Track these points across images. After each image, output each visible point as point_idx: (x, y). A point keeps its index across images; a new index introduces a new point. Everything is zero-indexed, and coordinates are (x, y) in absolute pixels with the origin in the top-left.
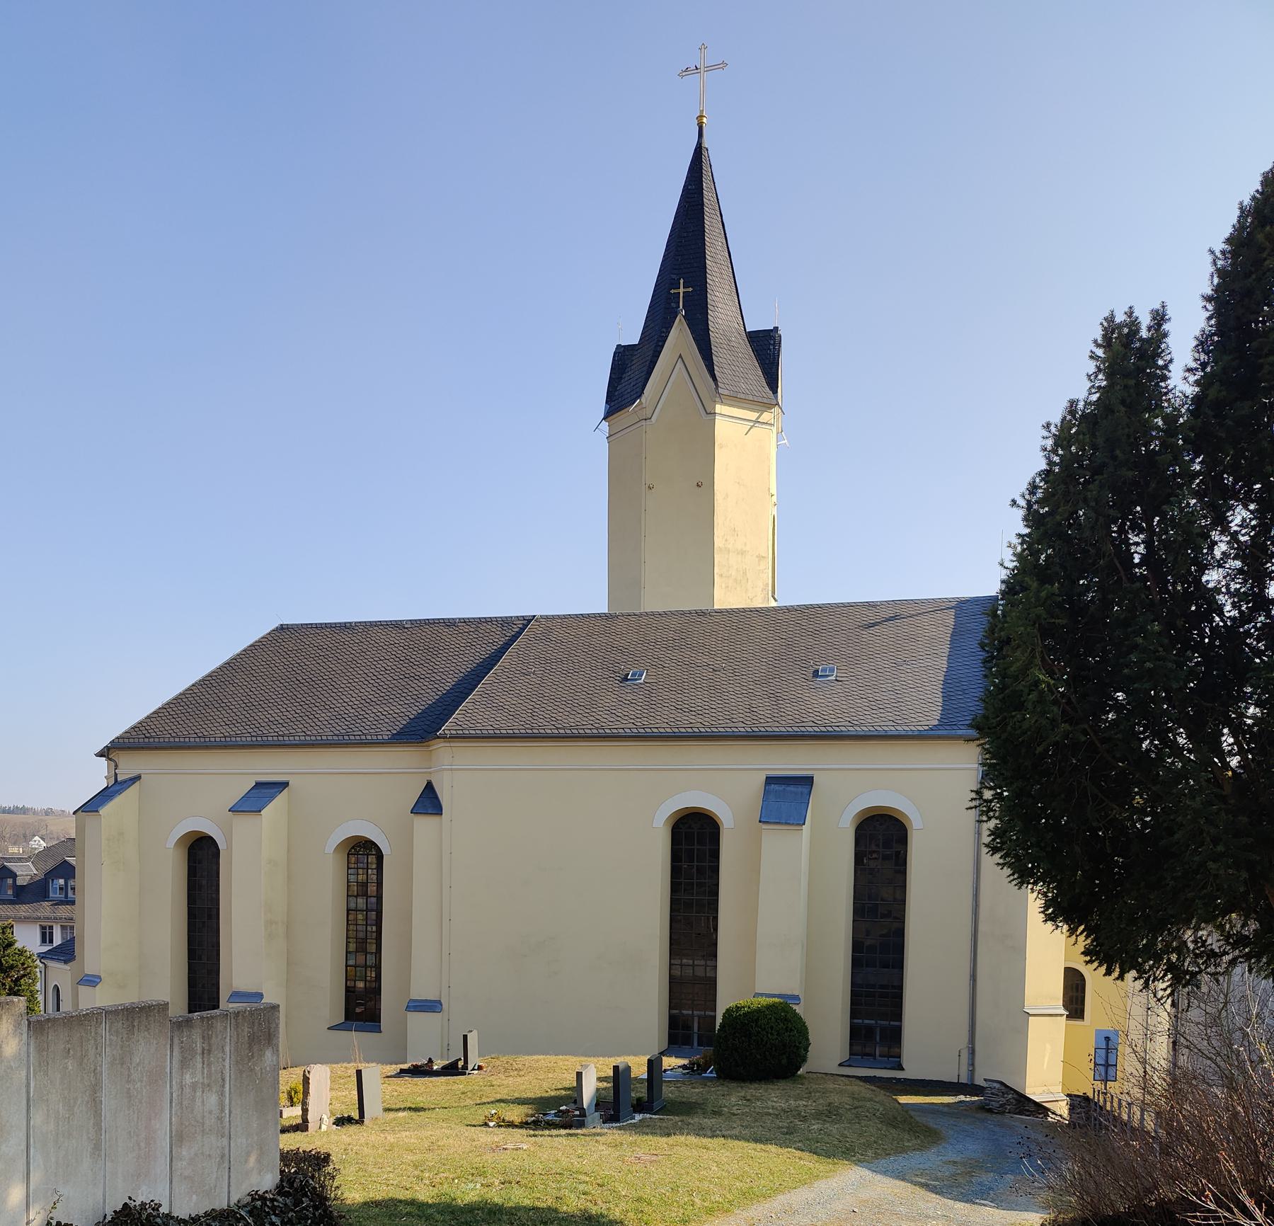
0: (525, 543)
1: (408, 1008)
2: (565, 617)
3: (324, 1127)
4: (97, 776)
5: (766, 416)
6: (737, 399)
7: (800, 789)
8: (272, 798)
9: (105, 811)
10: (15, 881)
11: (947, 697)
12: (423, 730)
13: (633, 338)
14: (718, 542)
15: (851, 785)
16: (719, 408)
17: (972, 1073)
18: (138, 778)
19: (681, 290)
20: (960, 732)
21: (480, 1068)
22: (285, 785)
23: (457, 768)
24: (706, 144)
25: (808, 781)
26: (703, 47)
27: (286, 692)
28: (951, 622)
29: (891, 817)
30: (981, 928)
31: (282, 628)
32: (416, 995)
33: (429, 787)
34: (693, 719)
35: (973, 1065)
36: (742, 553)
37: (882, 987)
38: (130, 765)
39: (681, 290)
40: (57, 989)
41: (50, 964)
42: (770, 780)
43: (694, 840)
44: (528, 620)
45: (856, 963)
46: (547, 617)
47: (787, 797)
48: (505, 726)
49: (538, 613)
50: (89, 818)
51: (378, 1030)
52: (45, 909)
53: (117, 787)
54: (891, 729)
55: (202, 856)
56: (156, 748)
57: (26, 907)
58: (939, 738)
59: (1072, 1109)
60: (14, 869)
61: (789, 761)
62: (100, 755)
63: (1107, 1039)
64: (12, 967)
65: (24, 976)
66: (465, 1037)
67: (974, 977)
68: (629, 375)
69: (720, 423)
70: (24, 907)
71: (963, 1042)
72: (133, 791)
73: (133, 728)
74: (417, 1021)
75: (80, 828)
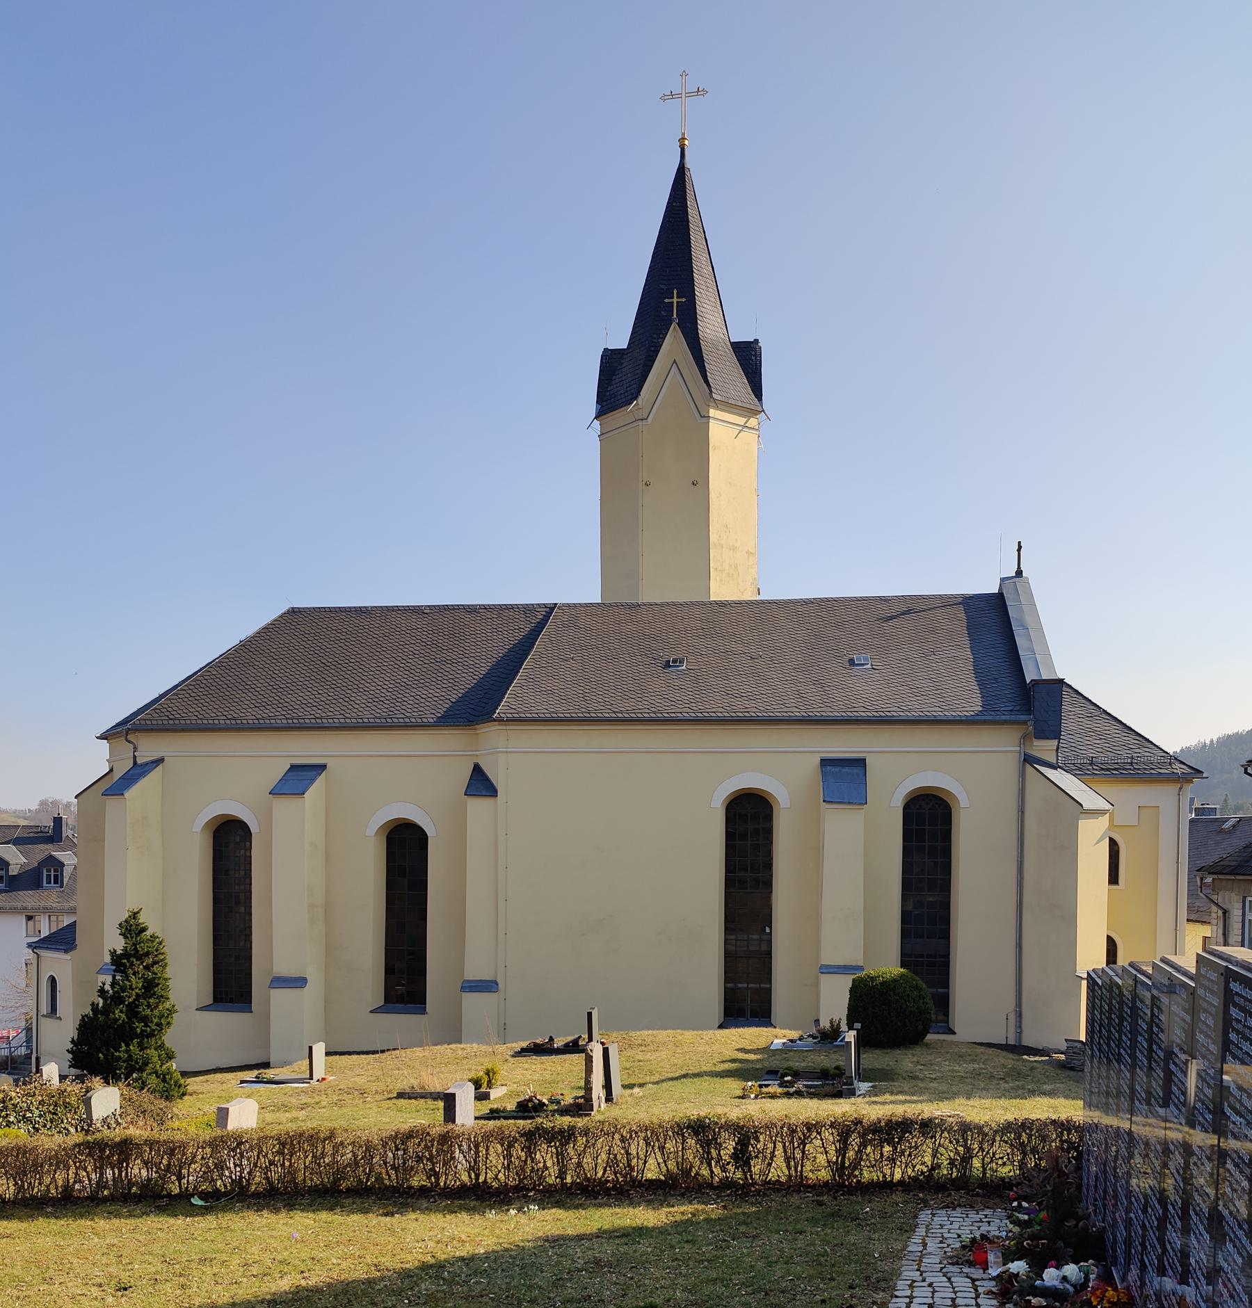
0: (522, 530)
1: (463, 989)
4: (96, 760)
5: (753, 422)
7: (855, 770)
8: (313, 780)
9: (131, 793)
10: (7, 871)
11: (982, 685)
12: (476, 708)
13: (621, 341)
15: (901, 768)
16: (712, 412)
17: (1019, 1033)
18: (161, 760)
19: (675, 300)
20: (1004, 717)
23: (505, 750)
24: (688, 164)
25: (861, 763)
26: (684, 74)
27: (301, 673)
28: (963, 616)
29: (928, 795)
30: (1025, 899)
31: (293, 611)
32: (826, 960)
33: (477, 771)
36: (734, 549)
37: (929, 956)
38: (149, 747)
39: (675, 300)
40: (53, 981)
41: (43, 953)
42: (825, 762)
43: (749, 819)
44: (551, 608)
45: (905, 934)
46: (569, 605)
47: (843, 778)
48: (561, 711)
50: (111, 803)
51: (423, 1011)
53: (138, 770)
54: (939, 714)
56: (183, 730)
58: (985, 722)
64: (147, 954)
66: (590, 1014)
67: (1019, 945)
68: (620, 380)
69: (713, 425)
71: (1010, 1005)
72: (155, 775)
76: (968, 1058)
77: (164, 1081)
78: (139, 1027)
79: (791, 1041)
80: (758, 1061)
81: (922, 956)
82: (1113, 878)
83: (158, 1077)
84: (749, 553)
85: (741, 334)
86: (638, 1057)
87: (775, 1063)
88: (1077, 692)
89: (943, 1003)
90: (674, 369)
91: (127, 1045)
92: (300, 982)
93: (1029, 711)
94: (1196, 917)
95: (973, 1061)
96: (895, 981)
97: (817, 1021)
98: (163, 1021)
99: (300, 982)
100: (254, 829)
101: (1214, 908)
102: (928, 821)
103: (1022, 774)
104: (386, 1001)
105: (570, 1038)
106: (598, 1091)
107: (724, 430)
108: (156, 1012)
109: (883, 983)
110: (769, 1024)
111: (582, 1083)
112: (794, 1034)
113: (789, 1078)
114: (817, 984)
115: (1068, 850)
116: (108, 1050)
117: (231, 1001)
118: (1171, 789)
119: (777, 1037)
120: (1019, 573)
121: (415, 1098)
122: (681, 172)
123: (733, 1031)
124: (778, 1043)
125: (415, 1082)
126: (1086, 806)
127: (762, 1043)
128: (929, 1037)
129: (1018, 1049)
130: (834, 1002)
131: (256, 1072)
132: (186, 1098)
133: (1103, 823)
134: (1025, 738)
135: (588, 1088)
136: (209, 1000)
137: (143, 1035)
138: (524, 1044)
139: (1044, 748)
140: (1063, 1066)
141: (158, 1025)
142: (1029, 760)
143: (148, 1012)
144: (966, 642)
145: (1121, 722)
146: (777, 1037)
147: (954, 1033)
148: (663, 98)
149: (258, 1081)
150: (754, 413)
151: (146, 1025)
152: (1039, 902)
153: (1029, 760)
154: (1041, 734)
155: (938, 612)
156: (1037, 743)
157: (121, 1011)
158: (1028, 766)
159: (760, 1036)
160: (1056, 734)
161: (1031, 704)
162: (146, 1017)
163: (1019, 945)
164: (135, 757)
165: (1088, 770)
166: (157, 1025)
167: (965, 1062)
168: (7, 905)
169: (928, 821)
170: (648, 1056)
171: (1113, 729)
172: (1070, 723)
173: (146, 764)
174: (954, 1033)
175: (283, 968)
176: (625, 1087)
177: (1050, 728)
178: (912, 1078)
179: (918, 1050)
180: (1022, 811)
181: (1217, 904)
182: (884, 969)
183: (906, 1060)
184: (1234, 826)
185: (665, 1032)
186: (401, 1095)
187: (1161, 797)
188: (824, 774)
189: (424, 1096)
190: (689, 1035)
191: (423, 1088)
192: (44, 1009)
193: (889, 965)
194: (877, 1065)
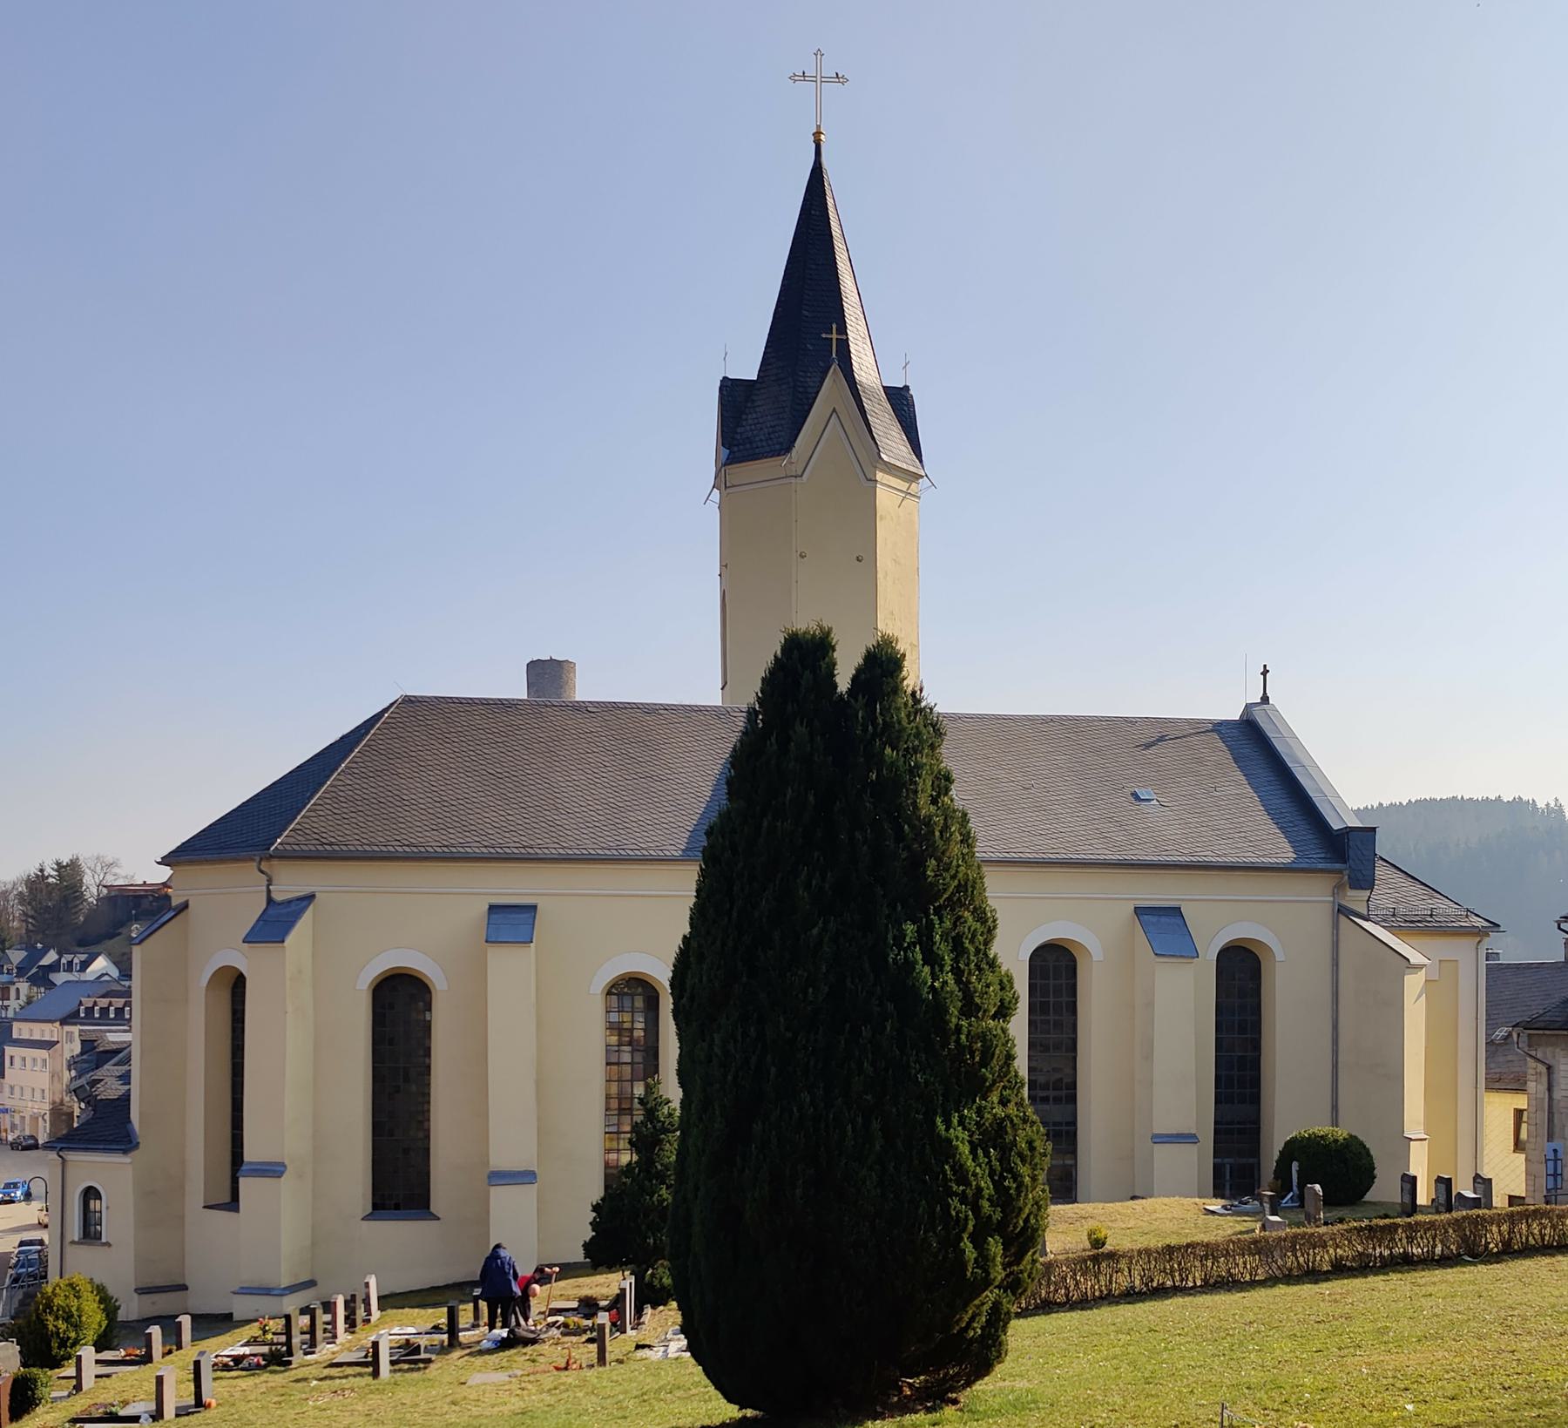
8: (306, 907)
15: (1218, 919)
16: (879, 476)
18: (310, 898)
31: (408, 701)
58: (1303, 870)
61: (1159, 891)
81: (1232, 1123)
102: (1241, 972)
103: (1336, 926)
107: (887, 493)
110: (1075, 1201)
117: (397, 1207)
118: (1470, 942)
120: (1265, 699)
122: (817, 174)
134: (1338, 888)
136: (369, 1209)
139: (1355, 899)
148: (793, 78)
152: (1370, 1062)
153: (1343, 911)
156: (1351, 893)
158: (1342, 919)
164: (269, 891)
165: (1414, 926)
169: (1241, 972)
175: (1189, 1153)
177: (1365, 881)
192: (75, 1231)
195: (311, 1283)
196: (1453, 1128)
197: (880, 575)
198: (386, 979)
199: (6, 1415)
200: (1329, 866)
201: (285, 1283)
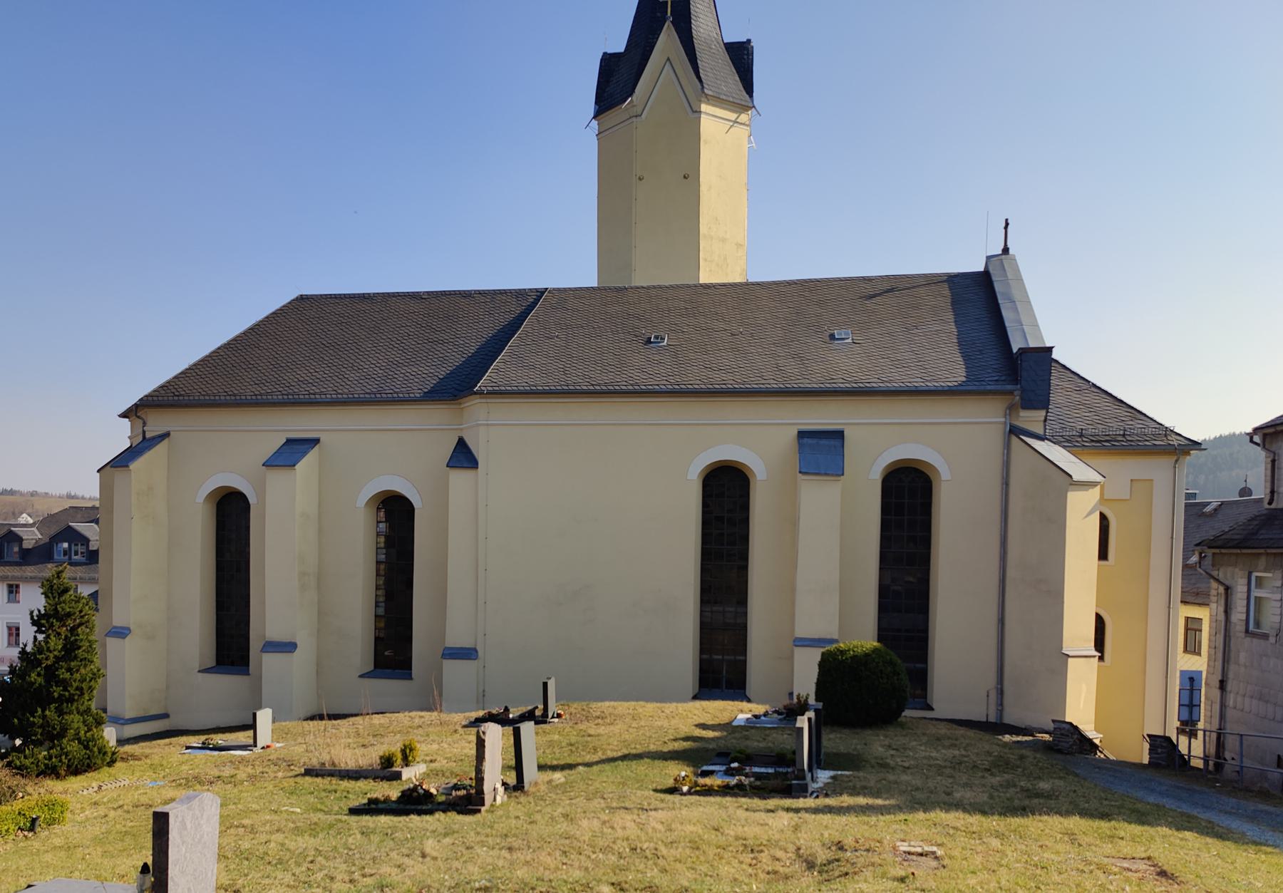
0: (529, 225)
1: (444, 656)
2: (576, 289)
3: (499, 799)
4: (120, 436)
5: (744, 118)
6: (719, 101)
7: (832, 442)
8: (305, 453)
9: (135, 466)
12: (457, 386)
13: (620, 47)
14: (703, 229)
16: (704, 107)
17: (1001, 711)
18: (167, 435)
20: (989, 387)
21: (559, 716)
22: (317, 441)
23: (486, 423)
25: (839, 435)
27: (302, 358)
30: (1010, 573)
31: (302, 298)
32: (800, 633)
33: (461, 443)
34: (724, 377)
35: (1002, 704)
36: (724, 240)
38: (157, 423)
42: (802, 434)
43: (726, 491)
44: (541, 293)
45: (883, 608)
46: (559, 290)
47: (821, 450)
48: (541, 383)
49: (550, 285)
50: (119, 474)
52: (49, 570)
53: (146, 444)
54: (919, 384)
55: (231, 511)
57: (32, 568)
59: (1152, 750)
60: (21, 534)
61: (821, 416)
62: (124, 415)
63: (1192, 679)
64: (69, 615)
65: (81, 624)
66: (545, 685)
67: (1001, 621)
68: (616, 80)
69: (705, 122)
70: (29, 568)
72: (161, 448)
73: (162, 387)
74: (452, 668)
75: (105, 487)
76: (947, 743)
77: (86, 747)
78: (57, 691)
79: (756, 716)
80: (713, 739)
82: (1103, 555)
83: (80, 742)
84: (739, 245)
85: (733, 35)
86: (592, 732)
87: (734, 743)
88: (1064, 367)
89: (921, 678)
90: (668, 66)
91: (43, 711)
92: (290, 647)
93: (1016, 381)
94: (1192, 596)
95: (953, 746)
96: (867, 655)
97: (791, 694)
98: (84, 685)
99: (290, 647)
100: (252, 500)
101: (1214, 584)
102: (908, 494)
103: (1008, 446)
104: (375, 666)
105: (530, 708)
106: (494, 777)
108: (77, 676)
109: (854, 657)
111: (513, 763)
112: (760, 709)
113: (735, 765)
114: (791, 657)
115: (1056, 523)
116: (24, 715)
117: (232, 664)
119: (741, 712)
120: (1006, 250)
121: (323, 776)
123: (705, 703)
124: (742, 717)
125: (325, 757)
126: (1075, 478)
127: (724, 718)
128: (907, 713)
129: (998, 727)
130: (805, 680)
131: (203, 738)
132: (118, 764)
133: (1095, 493)
134: (1011, 409)
135: (480, 780)
136: (211, 662)
137: (61, 700)
138: (481, 713)
139: (1031, 419)
140: (1047, 747)
141: (80, 689)
142: (1015, 431)
143: (67, 675)
144: (950, 316)
145: (1111, 395)
146: (741, 712)
147: (931, 709)
149: (205, 747)
150: (745, 108)
151: (65, 689)
152: (1025, 581)
153: (1015, 431)
154: (1029, 404)
155: (922, 290)
156: (1024, 414)
157: (39, 675)
158: (1014, 439)
159: (725, 710)
160: (1043, 403)
161: (1016, 374)
162: (64, 680)
163: (1001, 621)
164: (144, 432)
165: (1078, 443)
166: (77, 689)
167: (944, 747)
168: (87, 576)
169: (908, 494)
170: (602, 730)
171: (1104, 403)
172: (1056, 397)
173: (153, 438)
174: (931, 709)
176: (541, 767)
177: (1038, 398)
178: (881, 765)
179: (891, 731)
180: (1006, 483)
181: (1217, 580)
182: (855, 643)
183: (877, 744)
184: (1215, 510)
185: (626, 704)
186: (309, 772)
187: (1156, 470)
188: (801, 446)
189: (331, 774)
190: (651, 707)
191: (333, 764)
193: (864, 638)
194: (842, 749)
195: (166, 716)
196: (1113, 650)
197: (702, 188)
198: (224, 497)
199: (1102, 613)
200: (999, 387)
201: (129, 714)
